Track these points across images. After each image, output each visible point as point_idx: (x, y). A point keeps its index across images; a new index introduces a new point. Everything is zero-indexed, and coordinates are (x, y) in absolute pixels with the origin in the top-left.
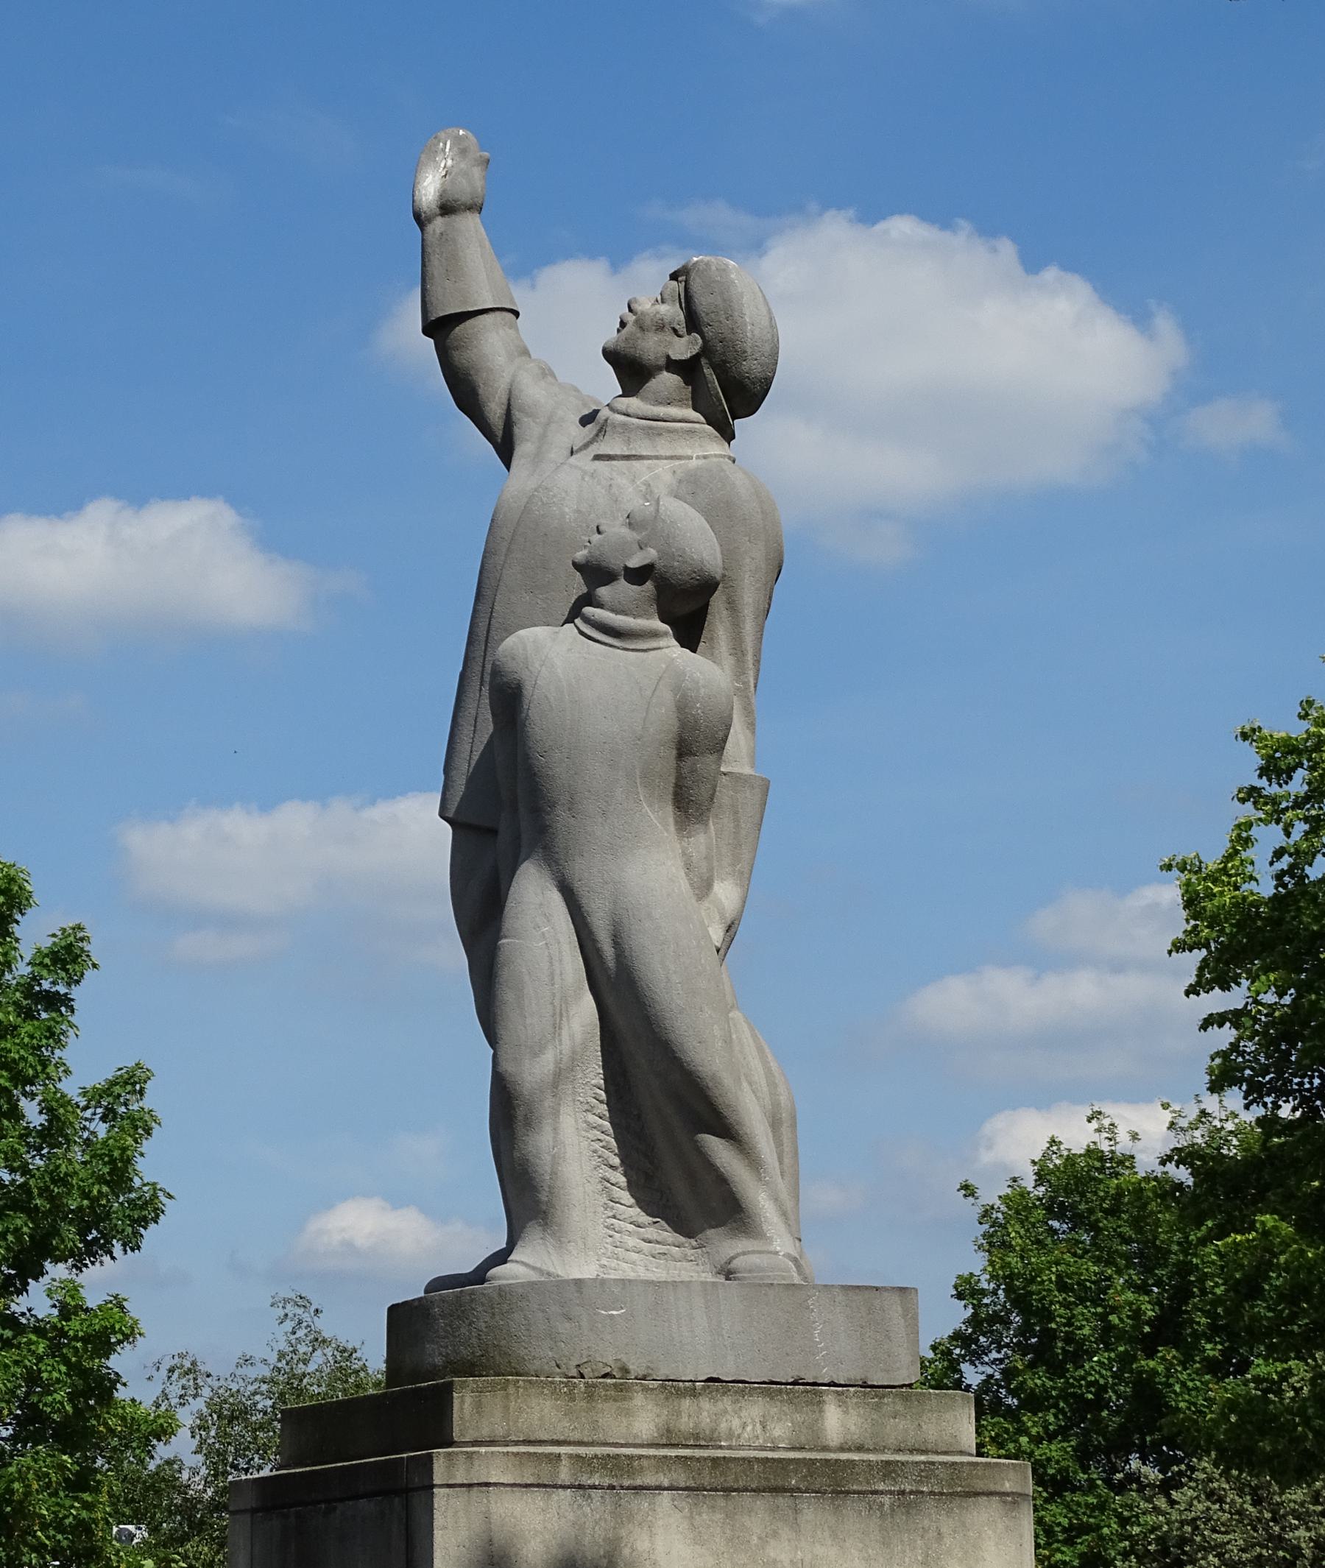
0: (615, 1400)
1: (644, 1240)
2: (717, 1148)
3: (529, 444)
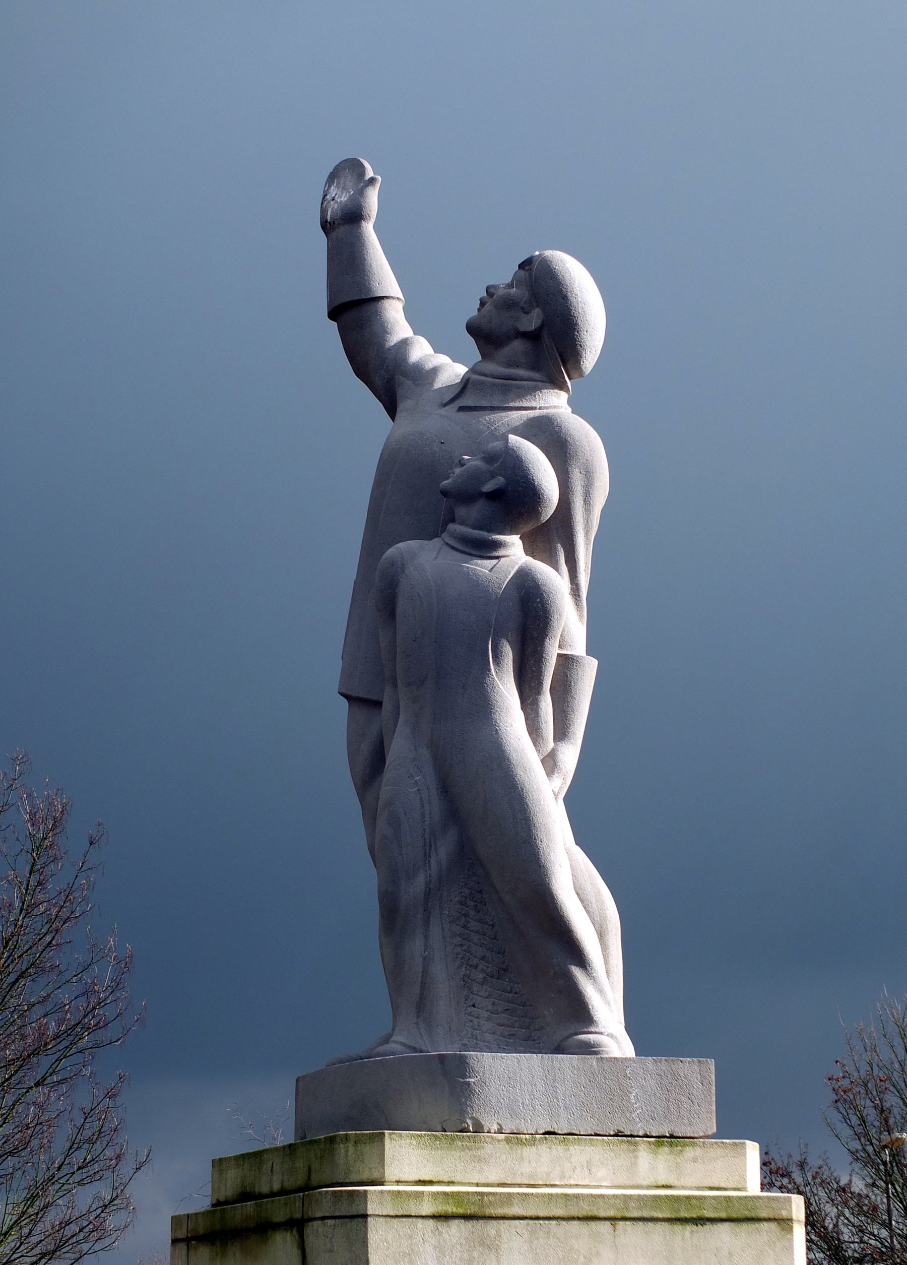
0: (470, 1149)
1: (498, 1025)
2: (577, 972)
3: (409, 401)
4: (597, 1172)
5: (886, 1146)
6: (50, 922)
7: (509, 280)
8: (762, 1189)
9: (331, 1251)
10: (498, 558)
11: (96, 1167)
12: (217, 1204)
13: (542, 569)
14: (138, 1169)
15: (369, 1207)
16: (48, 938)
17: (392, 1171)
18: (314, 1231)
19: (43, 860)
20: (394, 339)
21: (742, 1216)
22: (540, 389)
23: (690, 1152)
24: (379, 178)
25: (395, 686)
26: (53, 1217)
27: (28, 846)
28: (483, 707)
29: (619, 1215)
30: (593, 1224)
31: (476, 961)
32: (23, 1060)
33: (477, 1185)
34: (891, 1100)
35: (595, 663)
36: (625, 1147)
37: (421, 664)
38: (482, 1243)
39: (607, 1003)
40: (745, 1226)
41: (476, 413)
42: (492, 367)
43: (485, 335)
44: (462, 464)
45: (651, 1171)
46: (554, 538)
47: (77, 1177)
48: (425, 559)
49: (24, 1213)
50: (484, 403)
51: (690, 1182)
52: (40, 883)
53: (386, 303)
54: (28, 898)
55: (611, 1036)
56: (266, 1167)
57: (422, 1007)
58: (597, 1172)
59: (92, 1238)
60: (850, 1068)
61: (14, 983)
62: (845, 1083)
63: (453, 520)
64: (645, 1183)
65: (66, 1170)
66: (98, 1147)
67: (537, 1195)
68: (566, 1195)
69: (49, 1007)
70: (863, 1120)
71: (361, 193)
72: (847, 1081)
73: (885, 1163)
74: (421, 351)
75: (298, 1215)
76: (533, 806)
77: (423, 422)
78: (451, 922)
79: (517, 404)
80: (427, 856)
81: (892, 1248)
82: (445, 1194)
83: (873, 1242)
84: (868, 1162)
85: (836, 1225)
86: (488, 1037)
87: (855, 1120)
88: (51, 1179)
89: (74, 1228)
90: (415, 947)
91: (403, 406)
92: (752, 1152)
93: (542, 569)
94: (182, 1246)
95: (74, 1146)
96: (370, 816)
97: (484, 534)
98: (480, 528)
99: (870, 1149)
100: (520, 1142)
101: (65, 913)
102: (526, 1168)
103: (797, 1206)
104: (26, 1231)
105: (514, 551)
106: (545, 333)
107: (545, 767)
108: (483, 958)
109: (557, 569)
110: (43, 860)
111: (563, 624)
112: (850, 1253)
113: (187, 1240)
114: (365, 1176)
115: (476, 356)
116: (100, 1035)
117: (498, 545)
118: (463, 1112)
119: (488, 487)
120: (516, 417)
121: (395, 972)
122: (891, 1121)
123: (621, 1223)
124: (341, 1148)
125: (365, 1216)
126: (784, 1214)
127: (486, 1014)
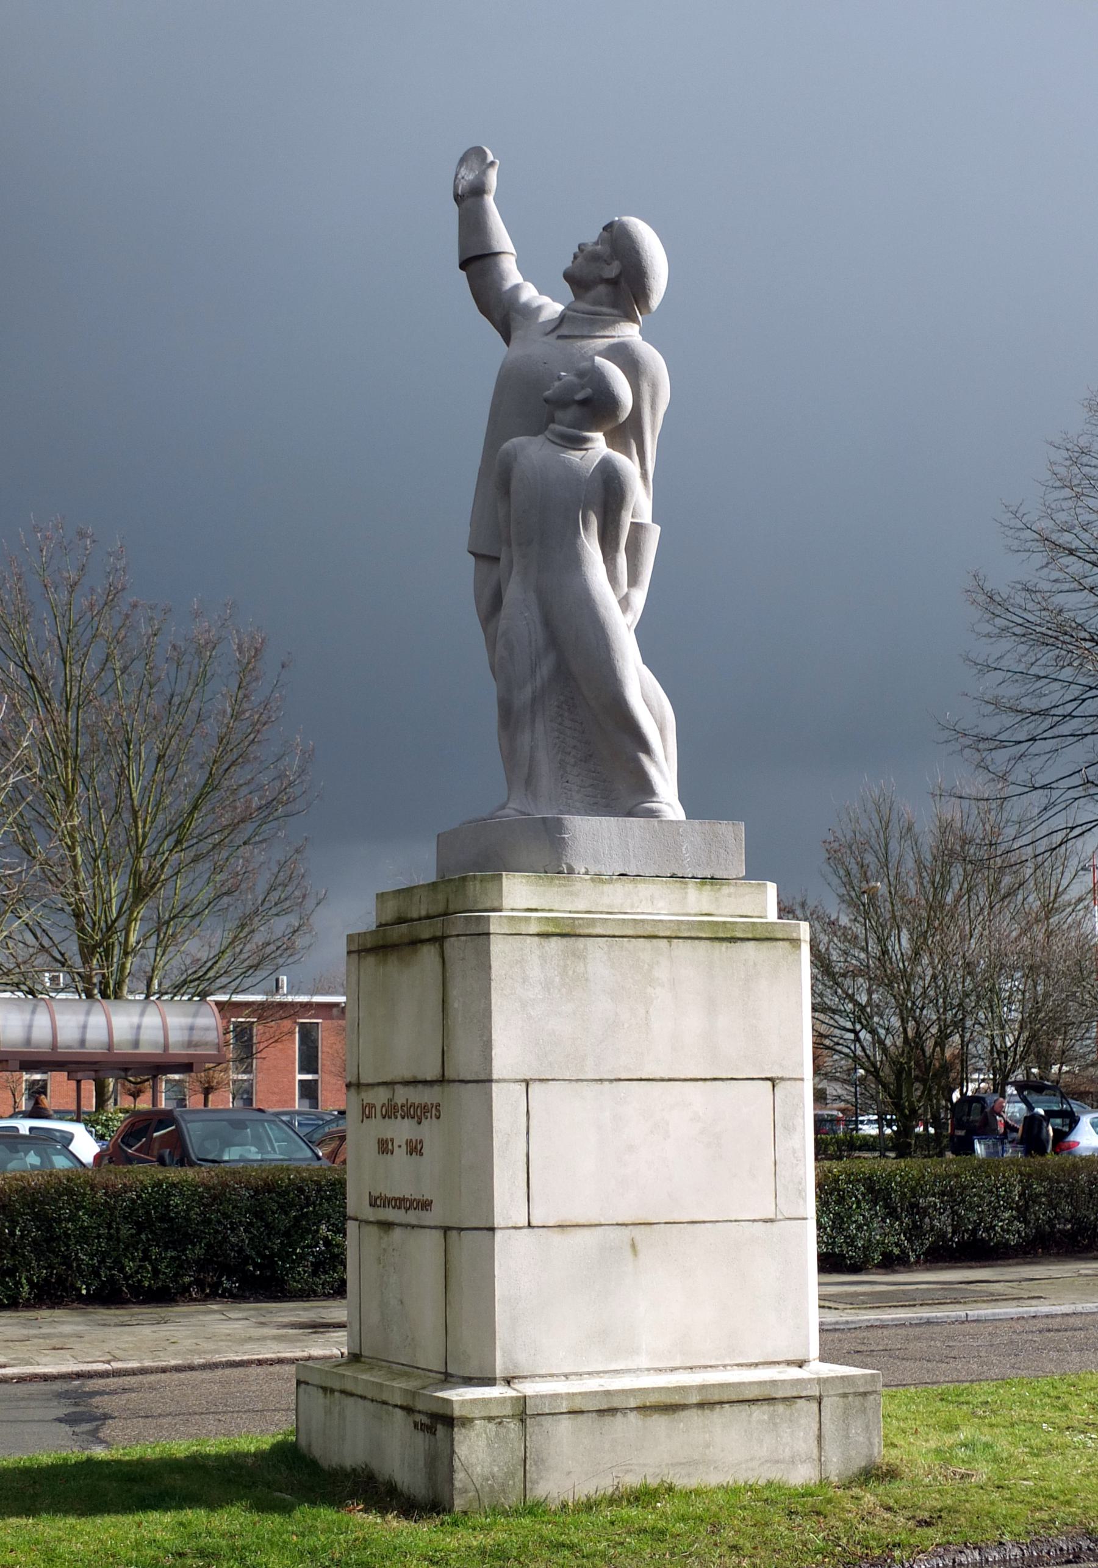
0: (565, 886)
2: (643, 757)
4: (657, 903)
5: (864, 892)
6: (254, 725)
7: (595, 239)
8: (780, 918)
9: (463, 959)
10: (586, 449)
11: (288, 904)
12: (380, 926)
13: (619, 458)
14: (318, 904)
15: (491, 927)
16: (252, 736)
17: (507, 903)
18: (453, 947)
19: (248, 679)
20: (509, 284)
21: (763, 937)
22: (618, 322)
23: (725, 890)
24: (497, 161)
25: (510, 546)
26: (259, 939)
27: (238, 668)
28: (575, 562)
29: (674, 935)
30: (654, 941)
31: (569, 750)
32: (234, 826)
33: (570, 912)
34: (869, 858)
35: (658, 528)
36: (678, 885)
37: (528, 529)
38: (574, 955)
39: (666, 780)
40: (766, 944)
41: (570, 341)
42: (582, 306)
43: (578, 281)
44: (560, 378)
45: (697, 903)
46: (627, 434)
47: (274, 911)
48: (532, 451)
49: (236, 937)
50: (576, 333)
51: (725, 911)
52: (245, 696)
53: (503, 257)
54: (237, 707)
55: (668, 804)
56: (416, 899)
57: (530, 782)
58: (657, 903)
59: (285, 955)
60: (839, 834)
61: (227, 770)
62: (836, 845)
63: (553, 422)
64: (692, 912)
65: (267, 905)
66: (289, 889)
67: (614, 920)
68: (635, 920)
69: (252, 787)
70: (848, 874)
71: (484, 173)
72: (837, 844)
73: (864, 905)
74: (529, 293)
75: (439, 934)
76: (613, 637)
77: (531, 347)
78: (551, 721)
79: (601, 334)
80: (533, 672)
81: (868, 967)
82: (547, 918)
83: (854, 962)
84: (852, 903)
85: (827, 949)
86: (578, 804)
87: (842, 873)
88: (256, 912)
89: (272, 947)
90: (525, 739)
91: (515, 335)
92: (772, 888)
93: (619, 458)
94: (355, 956)
95: (272, 888)
96: (491, 643)
97: (576, 431)
98: (574, 428)
99: (853, 894)
100: (602, 881)
101: (264, 718)
102: (606, 900)
103: (804, 930)
104: (238, 950)
105: (599, 445)
106: (622, 280)
107: (619, 603)
108: (574, 747)
109: (630, 457)
110: (248, 679)
111: (634, 499)
112: (837, 969)
113: (359, 952)
114: (488, 905)
115: (571, 297)
116: (291, 807)
117: (586, 440)
118: (559, 860)
119: (579, 396)
120: (601, 343)
121: (510, 757)
122: (869, 873)
123: (676, 941)
124: (470, 885)
125: (488, 934)
126: (795, 935)
127: (577, 788)
